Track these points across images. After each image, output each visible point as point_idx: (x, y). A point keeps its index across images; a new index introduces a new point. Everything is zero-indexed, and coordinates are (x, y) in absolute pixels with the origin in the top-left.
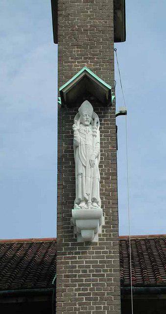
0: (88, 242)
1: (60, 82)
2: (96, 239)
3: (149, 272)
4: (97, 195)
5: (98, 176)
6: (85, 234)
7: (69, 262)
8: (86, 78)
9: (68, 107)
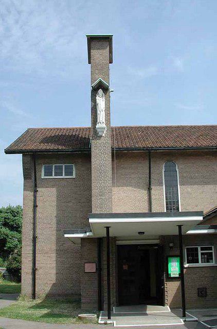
0: (101, 136)
1: (92, 82)
2: (104, 135)
3: (120, 143)
4: (104, 121)
5: (104, 115)
6: (100, 134)
7: (65, 175)
8: (100, 82)
9: (95, 91)
